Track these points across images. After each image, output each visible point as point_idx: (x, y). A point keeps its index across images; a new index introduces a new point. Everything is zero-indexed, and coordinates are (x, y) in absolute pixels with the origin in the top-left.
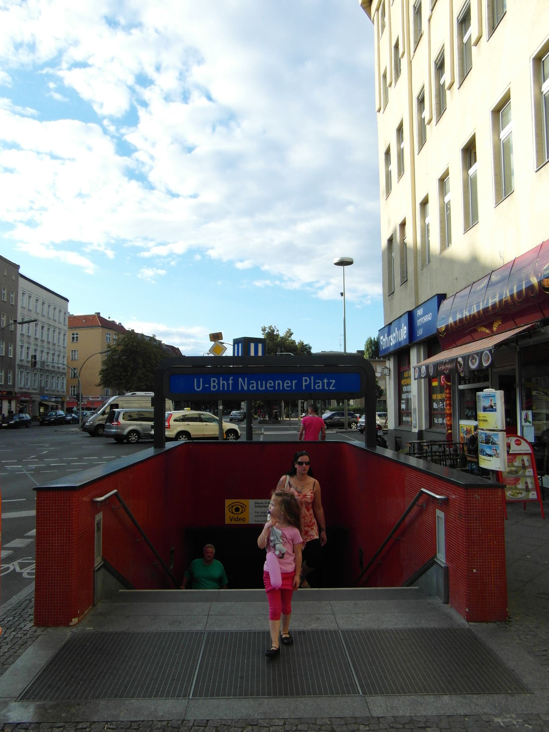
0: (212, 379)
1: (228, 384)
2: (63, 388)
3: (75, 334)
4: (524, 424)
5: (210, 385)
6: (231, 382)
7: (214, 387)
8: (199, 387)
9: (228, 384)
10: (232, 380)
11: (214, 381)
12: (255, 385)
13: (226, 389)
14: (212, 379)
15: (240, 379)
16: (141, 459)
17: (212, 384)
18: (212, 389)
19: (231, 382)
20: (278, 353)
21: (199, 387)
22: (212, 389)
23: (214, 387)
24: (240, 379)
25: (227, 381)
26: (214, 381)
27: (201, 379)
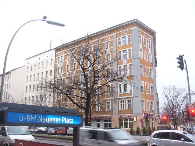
0: (28, 116)
1: (34, 118)
2: (123, 109)
3: (121, 104)
4: (127, 100)
5: (26, 119)
6: (35, 118)
7: (28, 120)
8: (21, 119)
9: (34, 118)
10: (36, 117)
11: (28, 117)
12: (45, 120)
13: (35, 121)
14: (28, 116)
15: (39, 117)
16: (52, 144)
17: (27, 118)
18: (27, 121)
19: (35, 118)
20: (68, 102)
21: (21, 119)
22: (27, 121)
23: (28, 120)
24: (39, 117)
25: (34, 117)
26: (28, 117)
27: (23, 115)
